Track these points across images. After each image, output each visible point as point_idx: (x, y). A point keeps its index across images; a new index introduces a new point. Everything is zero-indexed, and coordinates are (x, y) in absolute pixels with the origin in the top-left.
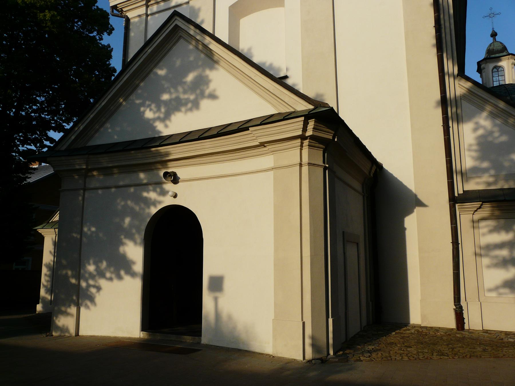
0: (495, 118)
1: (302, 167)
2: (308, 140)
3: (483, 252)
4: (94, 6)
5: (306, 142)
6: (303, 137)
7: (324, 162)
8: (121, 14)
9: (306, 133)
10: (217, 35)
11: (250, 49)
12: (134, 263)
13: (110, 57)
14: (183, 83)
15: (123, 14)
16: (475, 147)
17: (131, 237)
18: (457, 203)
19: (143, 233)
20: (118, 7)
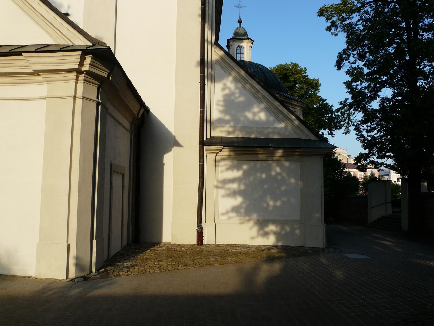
1: (76, 99)
2: (84, 75)
5: (82, 77)
6: (79, 72)
7: (98, 98)
16: (222, 103)
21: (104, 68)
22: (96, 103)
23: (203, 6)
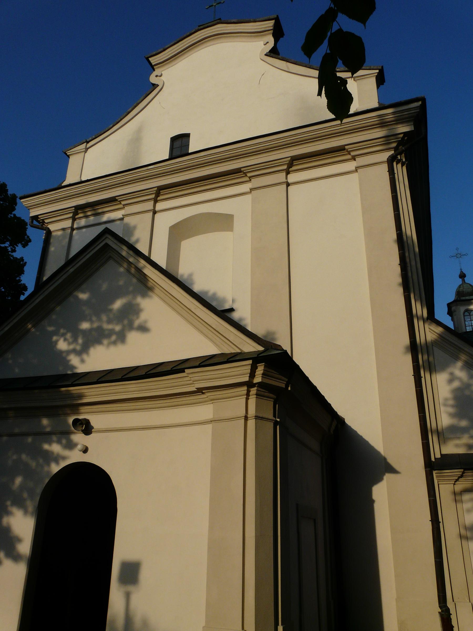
0: (471, 369)
1: (248, 420)
2: (256, 388)
3: (469, 534)
4: (12, 214)
5: (254, 391)
6: (249, 385)
7: (274, 416)
8: (42, 225)
9: (253, 379)
10: (153, 258)
11: (191, 275)
12: (19, 540)
13: (22, 272)
14: (108, 311)
15: (44, 226)
16: (451, 402)
17: (20, 503)
18: (435, 470)
19: (38, 498)
20: (39, 218)
21: (280, 377)
22: (273, 423)
23: (403, 272)
